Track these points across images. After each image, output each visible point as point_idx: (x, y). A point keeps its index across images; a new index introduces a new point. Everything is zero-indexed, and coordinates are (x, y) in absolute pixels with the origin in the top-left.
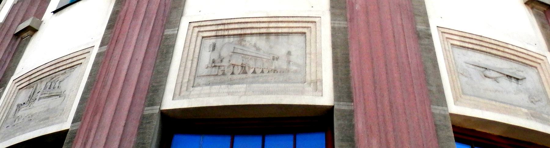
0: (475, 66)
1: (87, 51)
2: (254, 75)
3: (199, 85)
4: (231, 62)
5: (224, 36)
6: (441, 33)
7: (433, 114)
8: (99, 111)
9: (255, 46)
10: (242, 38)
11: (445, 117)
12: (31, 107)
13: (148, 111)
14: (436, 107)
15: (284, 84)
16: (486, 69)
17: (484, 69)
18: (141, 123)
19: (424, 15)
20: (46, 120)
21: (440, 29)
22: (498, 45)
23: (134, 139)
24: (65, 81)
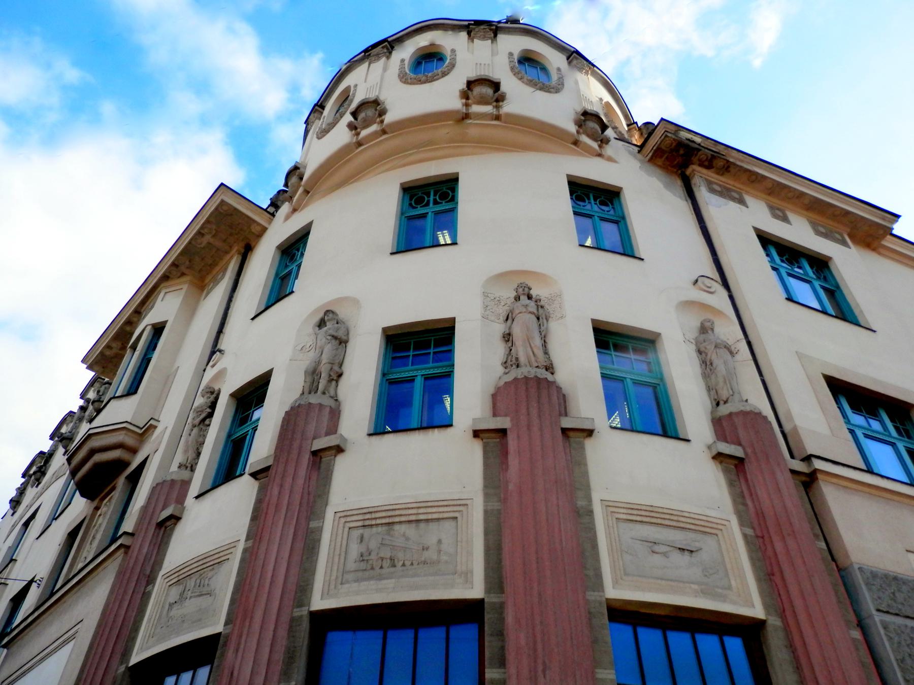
0: (643, 541)
1: (233, 545)
2: (404, 568)
3: (348, 582)
4: (379, 556)
5: (372, 526)
6: (605, 508)
7: (587, 602)
8: (247, 615)
9: (404, 535)
10: (390, 527)
11: (600, 603)
12: (183, 606)
13: (297, 613)
14: (592, 593)
15: (433, 577)
16: (655, 543)
17: (652, 544)
18: (291, 627)
19: (587, 488)
20: (198, 622)
21: (604, 502)
22: (672, 514)
23: (284, 642)
24: (214, 578)
